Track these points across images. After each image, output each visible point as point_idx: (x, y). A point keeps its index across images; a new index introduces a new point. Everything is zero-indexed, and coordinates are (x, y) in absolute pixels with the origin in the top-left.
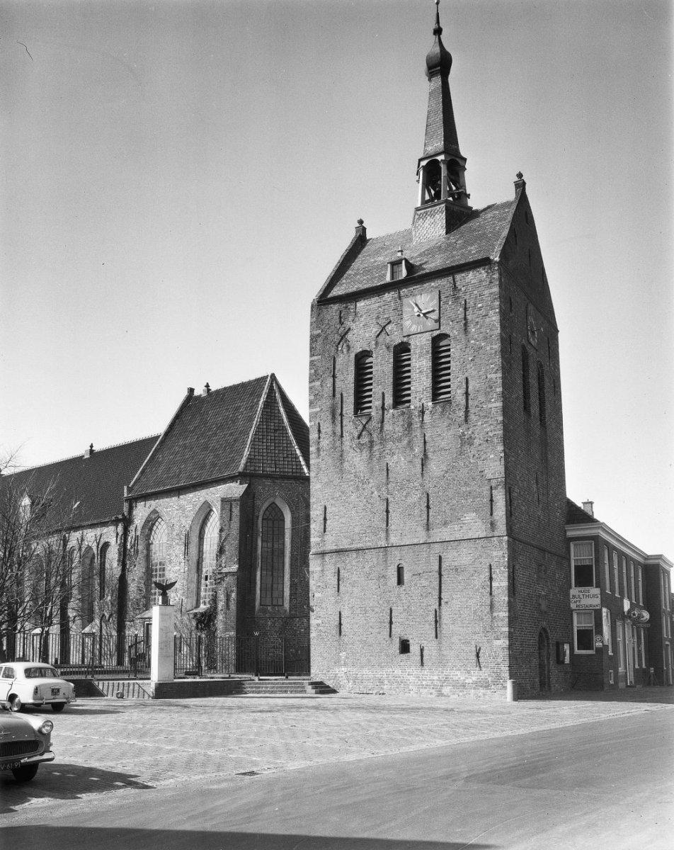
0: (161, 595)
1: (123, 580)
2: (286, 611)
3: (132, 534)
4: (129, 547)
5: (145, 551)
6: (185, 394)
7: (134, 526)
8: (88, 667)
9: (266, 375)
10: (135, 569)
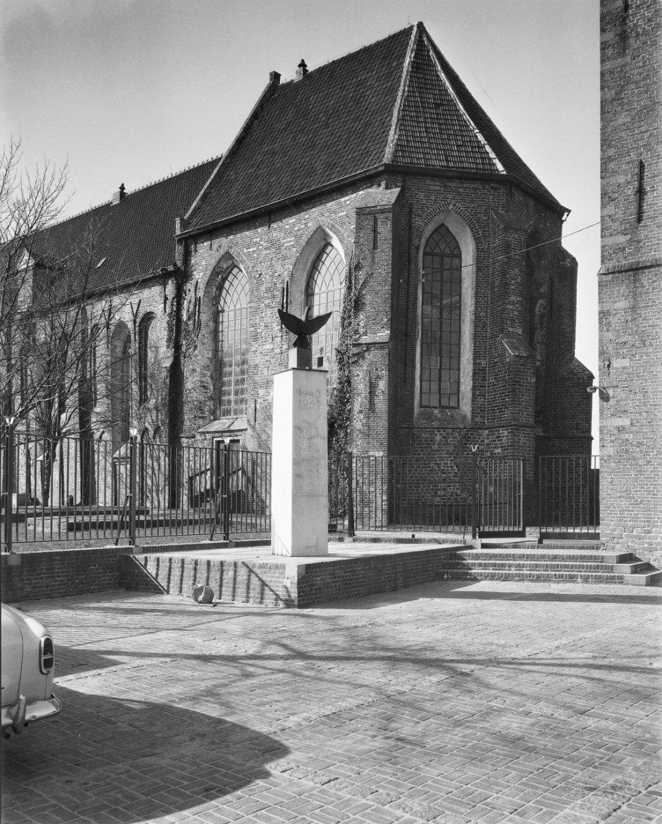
0: (295, 345)
1: (176, 372)
2: (464, 417)
3: (190, 296)
4: (185, 317)
5: (211, 324)
6: (265, 82)
7: (194, 282)
8: (122, 513)
9: (407, 26)
10: (196, 352)
